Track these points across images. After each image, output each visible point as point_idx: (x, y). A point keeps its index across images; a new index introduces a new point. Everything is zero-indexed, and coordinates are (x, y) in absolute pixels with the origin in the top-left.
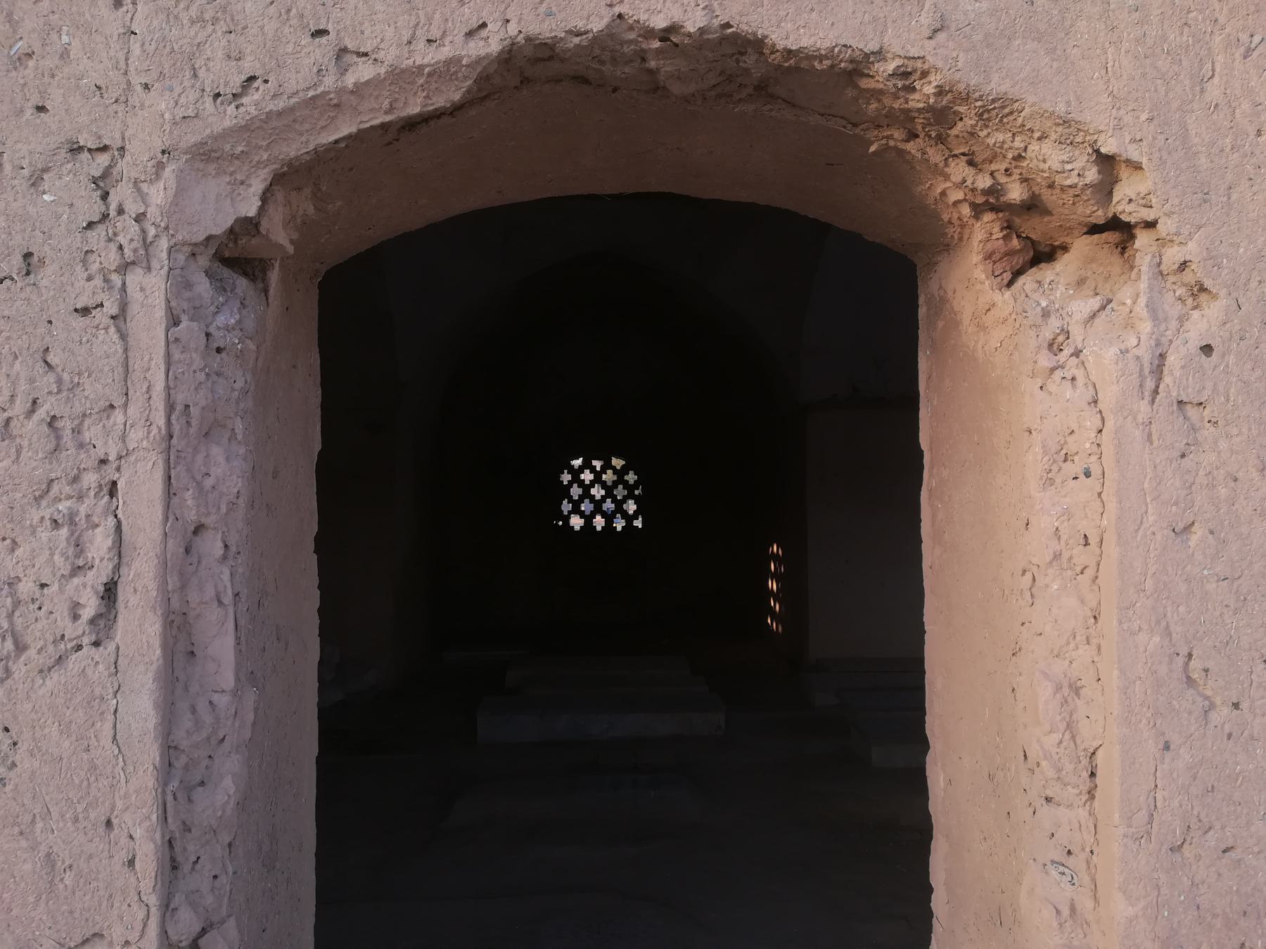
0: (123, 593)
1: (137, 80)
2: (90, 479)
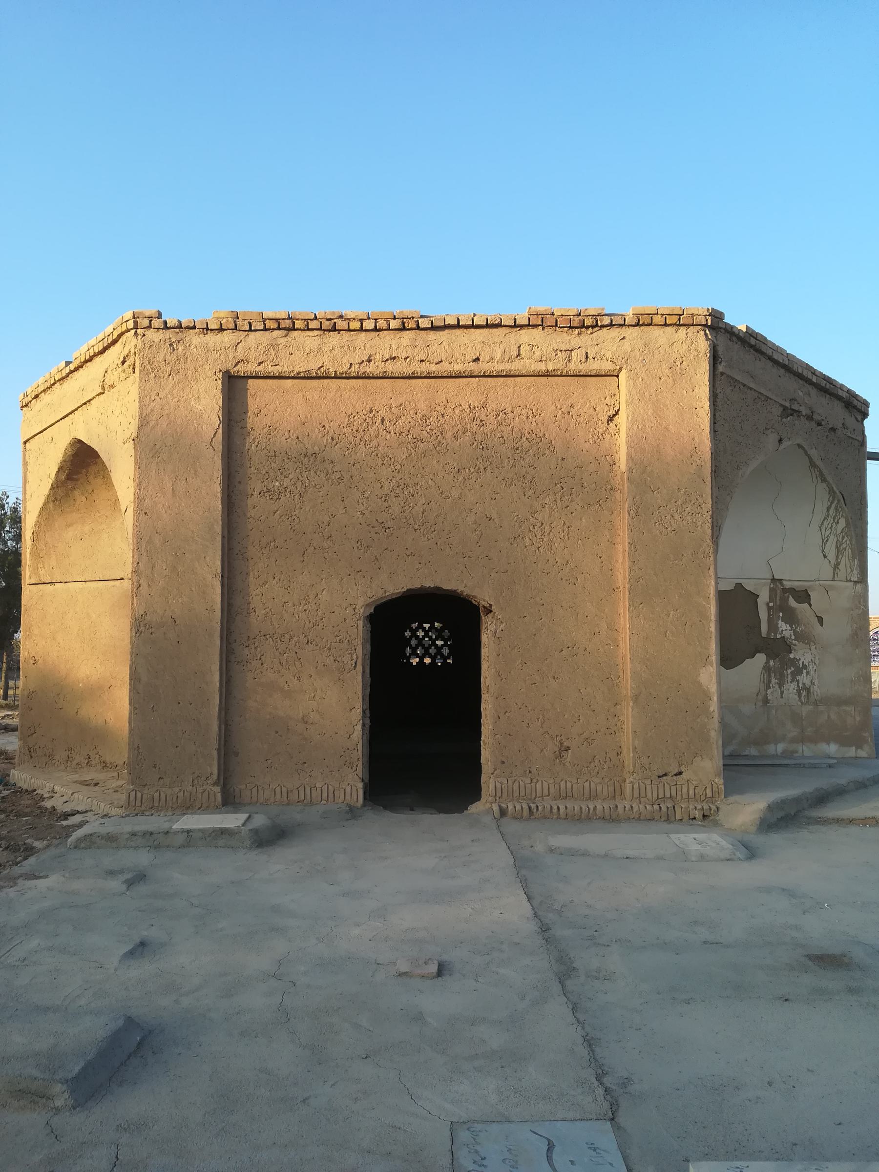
1: (359, 596)
2: (353, 648)
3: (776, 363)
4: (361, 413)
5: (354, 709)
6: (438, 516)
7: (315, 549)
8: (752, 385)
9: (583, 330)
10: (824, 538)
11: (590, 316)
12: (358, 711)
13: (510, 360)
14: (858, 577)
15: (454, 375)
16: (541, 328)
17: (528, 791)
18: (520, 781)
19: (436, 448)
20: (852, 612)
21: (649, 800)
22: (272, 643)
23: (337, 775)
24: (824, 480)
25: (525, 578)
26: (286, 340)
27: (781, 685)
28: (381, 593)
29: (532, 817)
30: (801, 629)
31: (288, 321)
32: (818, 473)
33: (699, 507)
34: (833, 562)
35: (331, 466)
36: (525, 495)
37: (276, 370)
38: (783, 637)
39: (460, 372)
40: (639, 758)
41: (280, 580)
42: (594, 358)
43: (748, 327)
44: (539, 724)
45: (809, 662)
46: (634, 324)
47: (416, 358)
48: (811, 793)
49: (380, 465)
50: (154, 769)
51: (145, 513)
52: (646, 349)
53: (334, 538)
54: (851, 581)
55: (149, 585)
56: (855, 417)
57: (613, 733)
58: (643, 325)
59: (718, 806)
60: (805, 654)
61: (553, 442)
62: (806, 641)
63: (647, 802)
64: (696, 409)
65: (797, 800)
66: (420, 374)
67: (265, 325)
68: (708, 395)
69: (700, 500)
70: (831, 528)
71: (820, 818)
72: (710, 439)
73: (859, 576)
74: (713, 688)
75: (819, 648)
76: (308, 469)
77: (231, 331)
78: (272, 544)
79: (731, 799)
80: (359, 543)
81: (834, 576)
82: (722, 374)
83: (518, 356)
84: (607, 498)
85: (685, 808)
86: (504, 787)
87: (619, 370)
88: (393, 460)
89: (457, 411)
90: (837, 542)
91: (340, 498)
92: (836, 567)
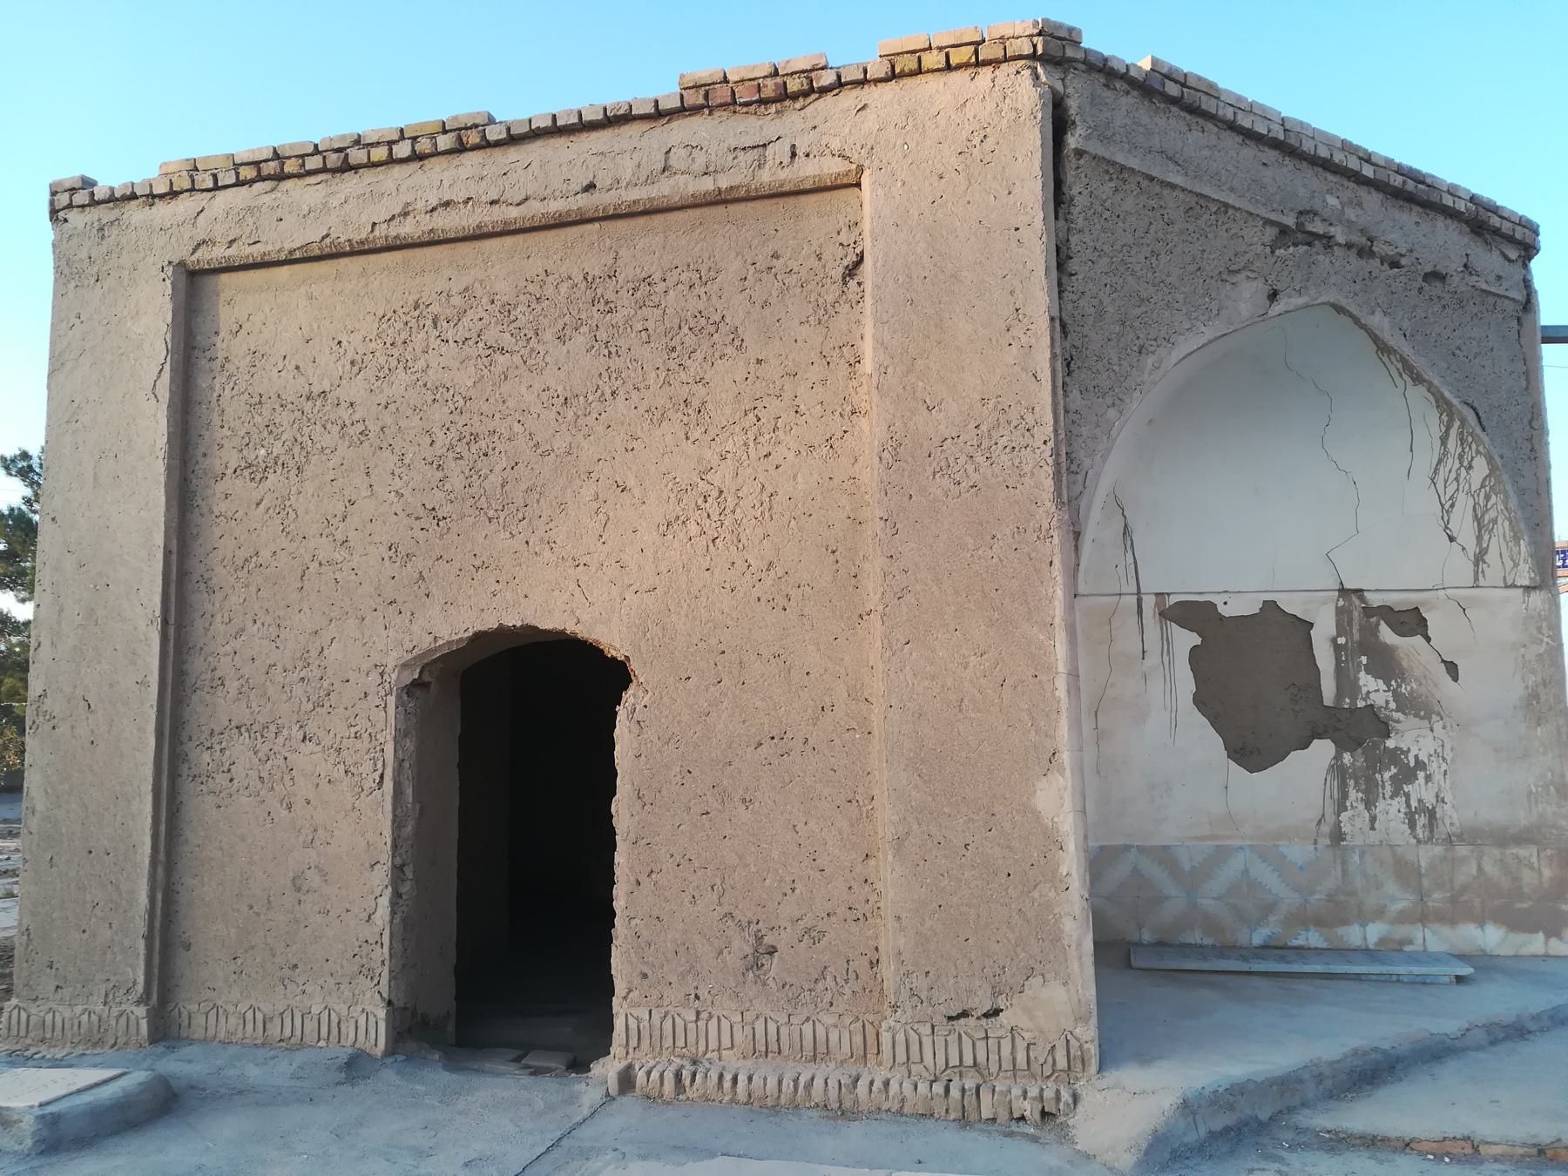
0: (385, 776)
2: (378, 748)
3: (1250, 135)
4: (400, 311)
5: (378, 866)
6: (529, 490)
7: (320, 564)
8: (1178, 180)
9: (787, 103)
10: (1444, 502)
11: (796, 73)
12: (385, 868)
13: (650, 180)
14: (1530, 578)
15: (552, 222)
16: (706, 111)
17: (691, 1038)
18: (676, 1016)
19: (525, 362)
20: (1523, 650)
21: (927, 1070)
22: (247, 740)
23: (347, 993)
24: (1418, 379)
25: (688, 601)
26: (273, 196)
27: (1369, 803)
28: (426, 643)
29: (681, 1097)
30: (1409, 688)
31: (272, 164)
32: (1400, 366)
33: (1027, 434)
34: (1472, 548)
35: (350, 411)
36: (687, 438)
37: (256, 252)
38: (1371, 705)
39: (560, 215)
40: (907, 974)
41: (263, 624)
42: (807, 155)
43: (1155, 61)
44: (715, 897)
45: (1431, 756)
46: (883, 75)
47: (483, 197)
48: (1331, 1063)
49: (430, 402)
50: (48, 970)
51: (53, 519)
52: (910, 120)
53: (351, 544)
54: (1516, 586)
55: (53, 643)
56: (1501, 251)
57: (861, 917)
58: (903, 75)
59: (1079, 1091)
60: (1420, 739)
61: (740, 331)
62: (1422, 713)
63: (925, 1074)
64: (1017, 229)
65: (1285, 1084)
66: (493, 227)
67: (237, 174)
68: (1040, 198)
69: (1030, 419)
70: (1457, 479)
71: (1328, 1132)
72: (1046, 290)
73: (1533, 575)
74: (1067, 825)
75: (1451, 726)
76: (312, 421)
77: (188, 194)
78: (254, 560)
79: (1112, 1076)
80: (393, 550)
81: (1476, 579)
82: (1080, 153)
83: (664, 170)
84: (845, 432)
85: (1001, 1092)
86: (644, 1028)
87: (857, 173)
88: (451, 392)
89: (564, 289)
90: (1474, 507)
91: (362, 468)
92: (1479, 558)
